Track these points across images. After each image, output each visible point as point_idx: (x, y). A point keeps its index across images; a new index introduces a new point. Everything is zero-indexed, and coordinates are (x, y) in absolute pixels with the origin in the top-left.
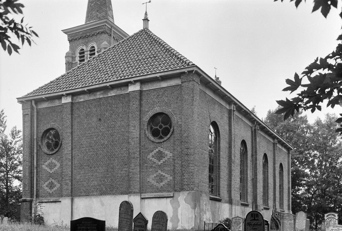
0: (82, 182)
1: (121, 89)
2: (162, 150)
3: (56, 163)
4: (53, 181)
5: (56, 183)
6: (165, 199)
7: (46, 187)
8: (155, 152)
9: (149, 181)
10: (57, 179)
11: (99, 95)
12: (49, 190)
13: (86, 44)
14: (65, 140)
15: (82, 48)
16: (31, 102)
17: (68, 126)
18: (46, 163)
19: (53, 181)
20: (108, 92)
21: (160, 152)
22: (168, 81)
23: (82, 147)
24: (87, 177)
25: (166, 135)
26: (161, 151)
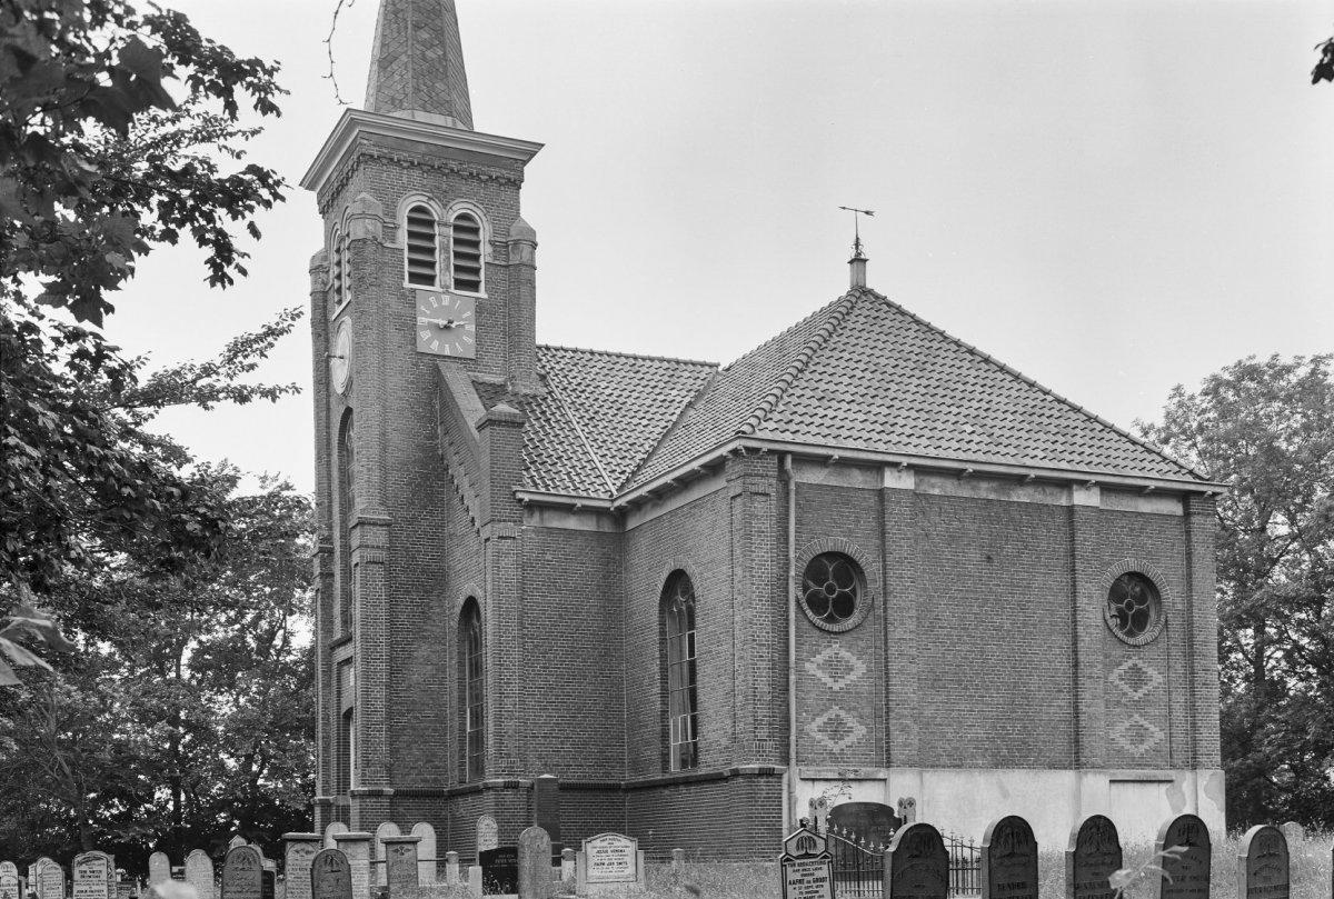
0: (941, 725)
1: (1044, 490)
2: (1140, 664)
3: (853, 660)
4: (843, 714)
5: (851, 721)
6: (1156, 785)
7: (820, 731)
8: (1125, 666)
9: (1113, 739)
10: (855, 709)
11: (985, 491)
12: (830, 744)
13: (445, 199)
14: (896, 597)
15: (423, 204)
16: (781, 461)
17: (906, 558)
18: (818, 656)
19: (843, 714)
20: (1013, 490)
21: (1136, 669)
22: (1154, 501)
23: (940, 627)
24: (954, 714)
25: (809, 602)
26: (1139, 666)
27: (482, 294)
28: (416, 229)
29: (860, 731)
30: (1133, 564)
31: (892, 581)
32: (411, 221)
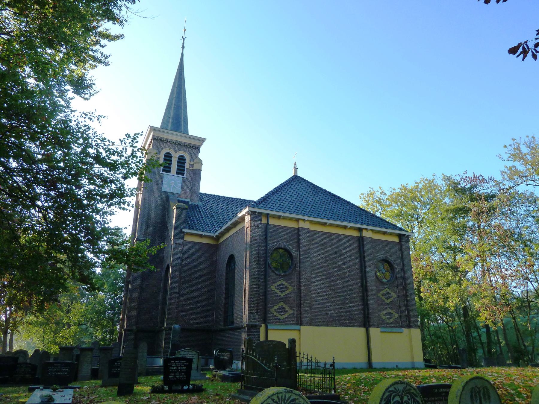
3: (288, 286)
4: (284, 305)
12: (279, 316)
27: (185, 176)
28: (179, 171)
29: (291, 312)
30: (383, 256)
31: (302, 258)
32: (165, 156)
